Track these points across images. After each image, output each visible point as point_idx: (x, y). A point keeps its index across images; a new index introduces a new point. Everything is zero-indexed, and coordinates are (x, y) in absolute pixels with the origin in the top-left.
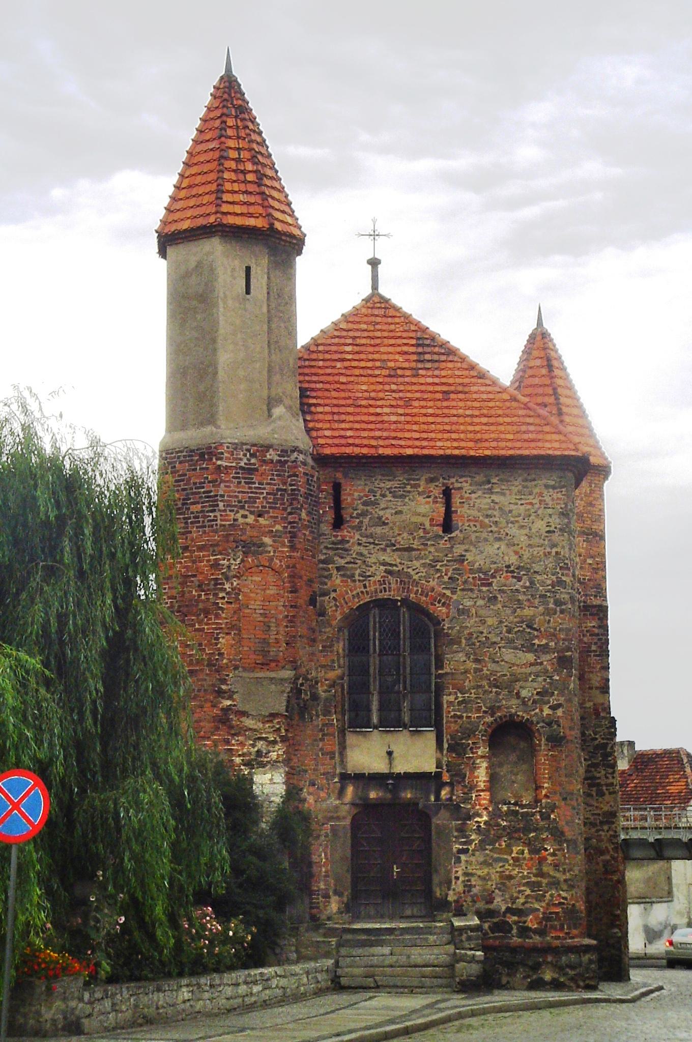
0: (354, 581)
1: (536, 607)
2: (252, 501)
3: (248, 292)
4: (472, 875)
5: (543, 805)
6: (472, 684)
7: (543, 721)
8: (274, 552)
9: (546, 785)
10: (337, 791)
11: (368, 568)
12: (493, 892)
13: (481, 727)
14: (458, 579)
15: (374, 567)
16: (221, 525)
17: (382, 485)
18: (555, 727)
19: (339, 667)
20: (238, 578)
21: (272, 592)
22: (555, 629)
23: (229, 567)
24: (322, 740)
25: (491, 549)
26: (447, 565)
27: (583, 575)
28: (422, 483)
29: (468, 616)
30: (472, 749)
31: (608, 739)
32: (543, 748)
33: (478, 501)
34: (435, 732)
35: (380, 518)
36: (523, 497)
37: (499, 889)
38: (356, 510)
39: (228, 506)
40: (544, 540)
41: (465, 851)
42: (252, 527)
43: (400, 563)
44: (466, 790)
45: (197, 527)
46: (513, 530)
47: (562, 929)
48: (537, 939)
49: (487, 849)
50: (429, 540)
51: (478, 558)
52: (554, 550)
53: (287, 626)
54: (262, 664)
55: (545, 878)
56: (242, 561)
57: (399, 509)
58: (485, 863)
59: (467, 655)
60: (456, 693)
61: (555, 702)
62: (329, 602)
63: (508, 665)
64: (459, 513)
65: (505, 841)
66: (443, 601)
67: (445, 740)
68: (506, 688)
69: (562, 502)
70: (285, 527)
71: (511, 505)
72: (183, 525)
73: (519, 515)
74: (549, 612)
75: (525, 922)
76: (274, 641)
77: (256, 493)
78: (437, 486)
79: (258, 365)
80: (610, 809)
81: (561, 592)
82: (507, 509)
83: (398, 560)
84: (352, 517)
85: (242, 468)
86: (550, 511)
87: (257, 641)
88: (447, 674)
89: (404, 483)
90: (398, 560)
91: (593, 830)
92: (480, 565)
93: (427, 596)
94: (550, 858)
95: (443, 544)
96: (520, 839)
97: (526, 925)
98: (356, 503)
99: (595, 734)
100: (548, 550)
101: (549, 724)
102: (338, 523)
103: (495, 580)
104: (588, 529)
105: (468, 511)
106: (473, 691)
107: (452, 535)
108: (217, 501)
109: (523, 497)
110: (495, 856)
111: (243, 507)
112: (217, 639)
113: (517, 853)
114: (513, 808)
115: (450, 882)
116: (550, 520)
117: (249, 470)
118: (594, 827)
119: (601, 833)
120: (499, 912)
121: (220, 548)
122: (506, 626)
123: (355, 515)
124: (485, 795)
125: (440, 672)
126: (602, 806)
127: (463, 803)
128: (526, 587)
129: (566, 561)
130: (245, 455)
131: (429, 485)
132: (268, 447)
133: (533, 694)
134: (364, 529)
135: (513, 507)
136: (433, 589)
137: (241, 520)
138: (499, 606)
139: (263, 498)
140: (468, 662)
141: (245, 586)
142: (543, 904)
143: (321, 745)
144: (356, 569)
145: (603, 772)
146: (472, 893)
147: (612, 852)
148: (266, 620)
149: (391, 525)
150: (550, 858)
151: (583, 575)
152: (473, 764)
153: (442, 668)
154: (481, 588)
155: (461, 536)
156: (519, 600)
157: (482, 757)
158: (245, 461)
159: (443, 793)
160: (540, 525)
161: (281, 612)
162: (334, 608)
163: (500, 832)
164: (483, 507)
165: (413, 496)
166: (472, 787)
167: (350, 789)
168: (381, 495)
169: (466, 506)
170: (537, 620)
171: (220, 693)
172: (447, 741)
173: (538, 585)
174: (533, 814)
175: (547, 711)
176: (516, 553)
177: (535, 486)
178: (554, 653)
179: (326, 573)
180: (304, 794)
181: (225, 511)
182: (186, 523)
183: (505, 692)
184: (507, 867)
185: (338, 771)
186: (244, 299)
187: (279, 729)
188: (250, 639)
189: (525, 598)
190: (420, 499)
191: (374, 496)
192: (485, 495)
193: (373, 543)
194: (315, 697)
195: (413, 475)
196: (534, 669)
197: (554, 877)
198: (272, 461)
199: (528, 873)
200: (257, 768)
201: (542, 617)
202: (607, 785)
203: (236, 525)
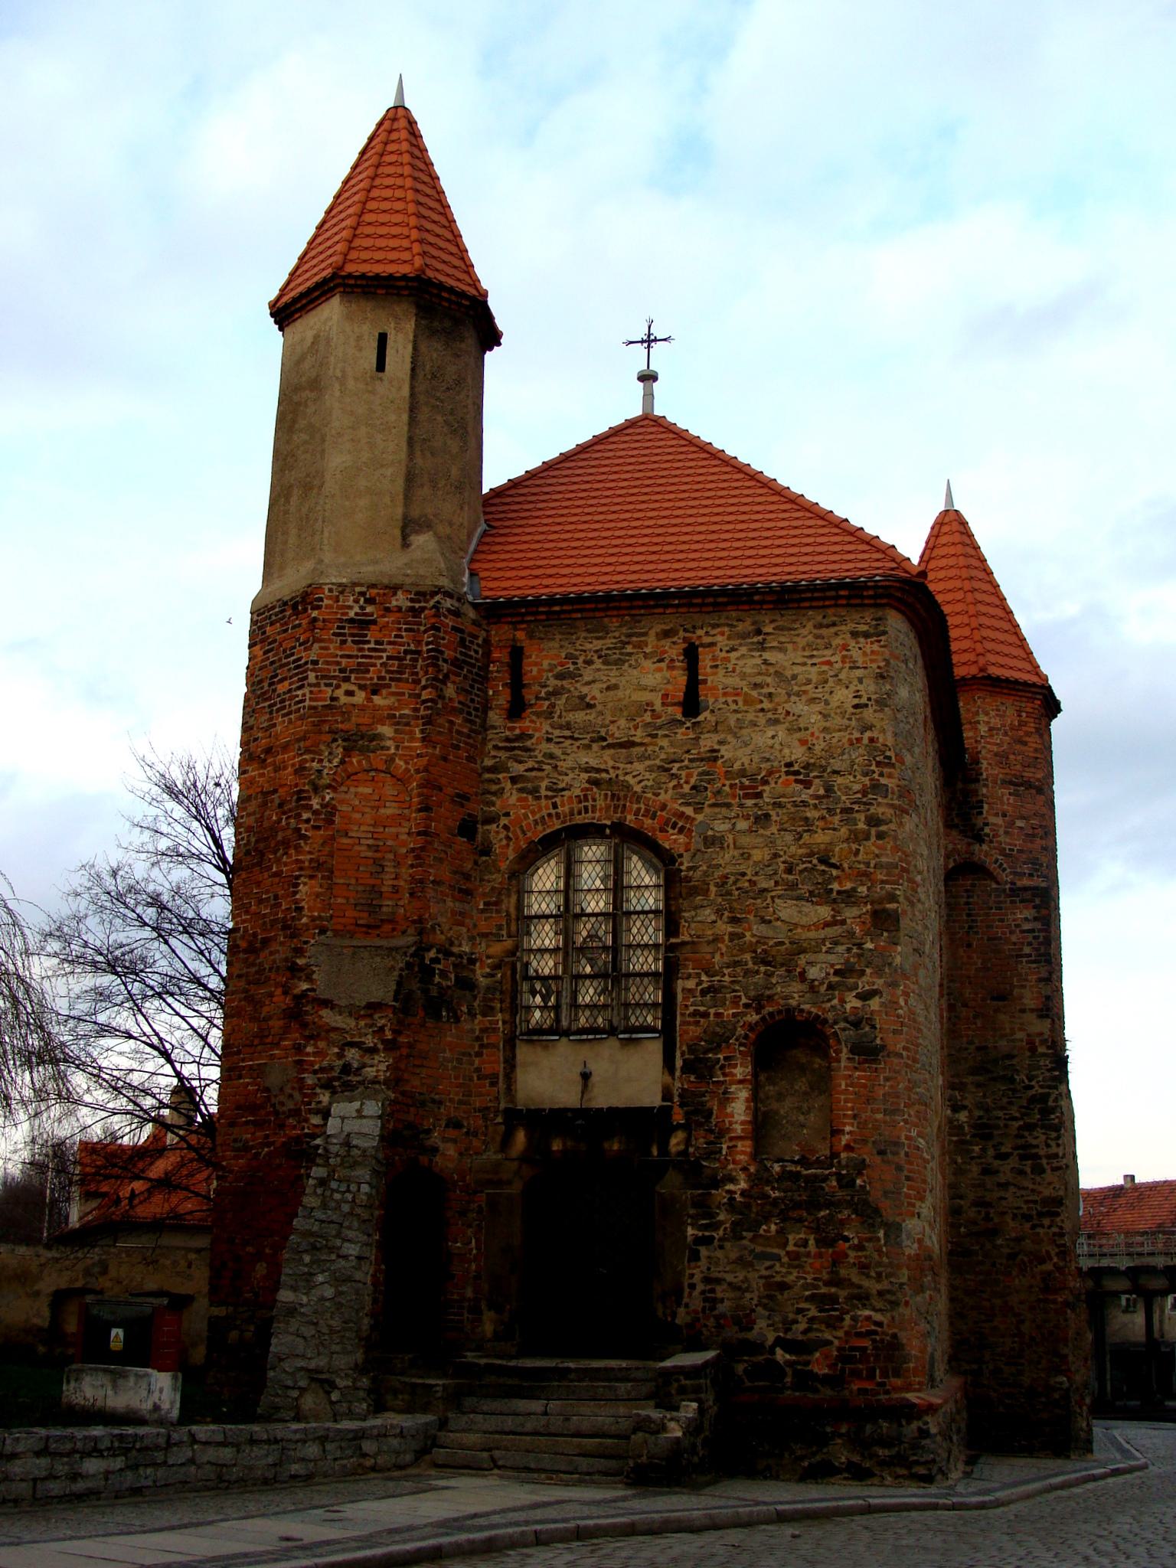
0: (538, 798)
1: (834, 829)
2: (362, 669)
3: (381, 366)
4: (719, 1281)
5: (844, 1162)
6: (726, 959)
7: (846, 1020)
8: (397, 748)
9: (848, 1128)
10: (498, 1139)
11: (561, 778)
12: (753, 1311)
13: (740, 1031)
14: (706, 789)
15: (571, 775)
16: (311, 708)
17: (588, 646)
18: (867, 1029)
19: (509, 936)
20: (334, 789)
21: (389, 812)
22: (868, 864)
23: (319, 771)
24: (479, 1054)
25: (762, 738)
26: (688, 768)
27: (1010, 844)
28: (651, 639)
29: (722, 848)
30: (722, 1067)
31: (1049, 1087)
32: (843, 1064)
33: (741, 663)
34: (662, 1039)
35: (582, 698)
36: (815, 653)
37: (765, 1307)
38: (546, 686)
39: (324, 677)
40: (850, 719)
41: (707, 1241)
42: (362, 708)
43: (613, 768)
44: (712, 1138)
45: (284, 716)
46: (799, 707)
47: (871, 1376)
48: (827, 1392)
49: (745, 1238)
50: (660, 728)
51: (739, 753)
52: (868, 734)
53: (412, 866)
54: (368, 926)
55: (843, 1289)
56: (342, 762)
57: (613, 681)
58: (740, 1261)
59: (719, 912)
60: (698, 975)
61: (867, 988)
62: (497, 833)
63: (785, 927)
64: (709, 683)
65: (776, 1224)
66: (680, 824)
67: (678, 1054)
68: (782, 965)
69: (880, 658)
70: (416, 710)
71: (794, 667)
72: (268, 716)
73: (809, 682)
74: (857, 837)
75: (807, 1363)
76: (390, 890)
77: (371, 657)
78: (674, 643)
79: (389, 472)
80: (1055, 1194)
81: (879, 804)
82: (788, 673)
83: (611, 763)
84: (537, 698)
85: (351, 621)
86: (859, 673)
87: (360, 888)
88: (684, 944)
89: (621, 642)
90: (611, 763)
91: (1028, 1225)
92: (743, 765)
93: (653, 817)
94: (852, 1254)
95: (683, 734)
96: (800, 1220)
97: (810, 1367)
98: (545, 674)
99: (1030, 1080)
100: (857, 735)
101: (856, 1024)
102: (517, 709)
103: (766, 788)
104: (1015, 776)
105: (723, 680)
106: (726, 971)
107: (698, 719)
108: (306, 671)
109: (815, 653)
110: (759, 1249)
111: (347, 679)
112: (296, 885)
113: (795, 1245)
114: (791, 1167)
115: (682, 1290)
116: (860, 687)
117: (363, 623)
118: (1028, 1221)
119: (1038, 1230)
120: (762, 1345)
121: (308, 743)
122: (784, 862)
123: (543, 694)
124: (745, 1147)
125: (673, 940)
126: (1040, 1188)
127: (705, 1159)
128: (818, 797)
129: (888, 753)
130: (356, 601)
131: (663, 642)
132: (394, 589)
133: (828, 974)
134: (556, 716)
135: (797, 670)
136: (664, 807)
137: (344, 699)
138: (774, 829)
139: (381, 664)
140: (719, 922)
141: (342, 802)
142: (840, 1333)
143: (477, 1061)
144: (542, 779)
145: (1043, 1137)
146: (716, 1312)
147: (1055, 1260)
148: (378, 855)
149: (599, 707)
150: (852, 1254)
151: (1010, 844)
152: (724, 1093)
153: (676, 934)
154: (744, 801)
155: (712, 719)
156: (807, 819)
157: (741, 1082)
158: (357, 609)
159: (673, 1141)
160: (843, 696)
161: (404, 844)
162: (504, 842)
163: (768, 1208)
164: (748, 670)
165: (636, 661)
166: (722, 1132)
167: (521, 1137)
168: (585, 662)
169: (721, 672)
170: (837, 849)
171: (294, 970)
172: (683, 1054)
173: (839, 793)
174: (825, 1179)
175: (852, 1003)
176: (803, 742)
177: (836, 634)
178: (866, 903)
179: (494, 788)
180: (435, 1138)
181: (317, 685)
182: (271, 713)
183: (782, 971)
184: (778, 1267)
185: (502, 1106)
186: (372, 378)
187: (382, 1029)
188: (348, 885)
189: (816, 814)
190: (648, 664)
191: (574, 663)
192: (754, 654)
193: (572, 738)
194: (466, 984)
195: (636, 627)
196: (831, 932)
197: (860, 1287)
198: (399, 609)
199: (815, 1279)
200: (342, 1092)
201: (845, 845)
202: (1049, 1157)
203: (335, 707)
